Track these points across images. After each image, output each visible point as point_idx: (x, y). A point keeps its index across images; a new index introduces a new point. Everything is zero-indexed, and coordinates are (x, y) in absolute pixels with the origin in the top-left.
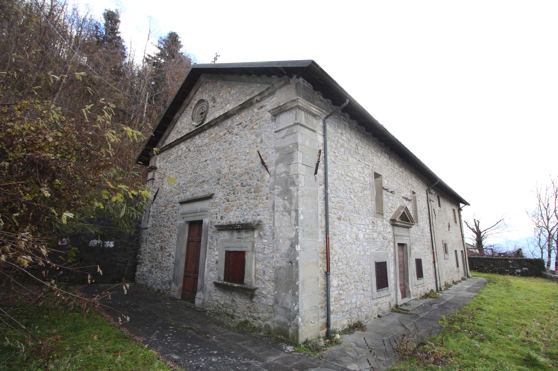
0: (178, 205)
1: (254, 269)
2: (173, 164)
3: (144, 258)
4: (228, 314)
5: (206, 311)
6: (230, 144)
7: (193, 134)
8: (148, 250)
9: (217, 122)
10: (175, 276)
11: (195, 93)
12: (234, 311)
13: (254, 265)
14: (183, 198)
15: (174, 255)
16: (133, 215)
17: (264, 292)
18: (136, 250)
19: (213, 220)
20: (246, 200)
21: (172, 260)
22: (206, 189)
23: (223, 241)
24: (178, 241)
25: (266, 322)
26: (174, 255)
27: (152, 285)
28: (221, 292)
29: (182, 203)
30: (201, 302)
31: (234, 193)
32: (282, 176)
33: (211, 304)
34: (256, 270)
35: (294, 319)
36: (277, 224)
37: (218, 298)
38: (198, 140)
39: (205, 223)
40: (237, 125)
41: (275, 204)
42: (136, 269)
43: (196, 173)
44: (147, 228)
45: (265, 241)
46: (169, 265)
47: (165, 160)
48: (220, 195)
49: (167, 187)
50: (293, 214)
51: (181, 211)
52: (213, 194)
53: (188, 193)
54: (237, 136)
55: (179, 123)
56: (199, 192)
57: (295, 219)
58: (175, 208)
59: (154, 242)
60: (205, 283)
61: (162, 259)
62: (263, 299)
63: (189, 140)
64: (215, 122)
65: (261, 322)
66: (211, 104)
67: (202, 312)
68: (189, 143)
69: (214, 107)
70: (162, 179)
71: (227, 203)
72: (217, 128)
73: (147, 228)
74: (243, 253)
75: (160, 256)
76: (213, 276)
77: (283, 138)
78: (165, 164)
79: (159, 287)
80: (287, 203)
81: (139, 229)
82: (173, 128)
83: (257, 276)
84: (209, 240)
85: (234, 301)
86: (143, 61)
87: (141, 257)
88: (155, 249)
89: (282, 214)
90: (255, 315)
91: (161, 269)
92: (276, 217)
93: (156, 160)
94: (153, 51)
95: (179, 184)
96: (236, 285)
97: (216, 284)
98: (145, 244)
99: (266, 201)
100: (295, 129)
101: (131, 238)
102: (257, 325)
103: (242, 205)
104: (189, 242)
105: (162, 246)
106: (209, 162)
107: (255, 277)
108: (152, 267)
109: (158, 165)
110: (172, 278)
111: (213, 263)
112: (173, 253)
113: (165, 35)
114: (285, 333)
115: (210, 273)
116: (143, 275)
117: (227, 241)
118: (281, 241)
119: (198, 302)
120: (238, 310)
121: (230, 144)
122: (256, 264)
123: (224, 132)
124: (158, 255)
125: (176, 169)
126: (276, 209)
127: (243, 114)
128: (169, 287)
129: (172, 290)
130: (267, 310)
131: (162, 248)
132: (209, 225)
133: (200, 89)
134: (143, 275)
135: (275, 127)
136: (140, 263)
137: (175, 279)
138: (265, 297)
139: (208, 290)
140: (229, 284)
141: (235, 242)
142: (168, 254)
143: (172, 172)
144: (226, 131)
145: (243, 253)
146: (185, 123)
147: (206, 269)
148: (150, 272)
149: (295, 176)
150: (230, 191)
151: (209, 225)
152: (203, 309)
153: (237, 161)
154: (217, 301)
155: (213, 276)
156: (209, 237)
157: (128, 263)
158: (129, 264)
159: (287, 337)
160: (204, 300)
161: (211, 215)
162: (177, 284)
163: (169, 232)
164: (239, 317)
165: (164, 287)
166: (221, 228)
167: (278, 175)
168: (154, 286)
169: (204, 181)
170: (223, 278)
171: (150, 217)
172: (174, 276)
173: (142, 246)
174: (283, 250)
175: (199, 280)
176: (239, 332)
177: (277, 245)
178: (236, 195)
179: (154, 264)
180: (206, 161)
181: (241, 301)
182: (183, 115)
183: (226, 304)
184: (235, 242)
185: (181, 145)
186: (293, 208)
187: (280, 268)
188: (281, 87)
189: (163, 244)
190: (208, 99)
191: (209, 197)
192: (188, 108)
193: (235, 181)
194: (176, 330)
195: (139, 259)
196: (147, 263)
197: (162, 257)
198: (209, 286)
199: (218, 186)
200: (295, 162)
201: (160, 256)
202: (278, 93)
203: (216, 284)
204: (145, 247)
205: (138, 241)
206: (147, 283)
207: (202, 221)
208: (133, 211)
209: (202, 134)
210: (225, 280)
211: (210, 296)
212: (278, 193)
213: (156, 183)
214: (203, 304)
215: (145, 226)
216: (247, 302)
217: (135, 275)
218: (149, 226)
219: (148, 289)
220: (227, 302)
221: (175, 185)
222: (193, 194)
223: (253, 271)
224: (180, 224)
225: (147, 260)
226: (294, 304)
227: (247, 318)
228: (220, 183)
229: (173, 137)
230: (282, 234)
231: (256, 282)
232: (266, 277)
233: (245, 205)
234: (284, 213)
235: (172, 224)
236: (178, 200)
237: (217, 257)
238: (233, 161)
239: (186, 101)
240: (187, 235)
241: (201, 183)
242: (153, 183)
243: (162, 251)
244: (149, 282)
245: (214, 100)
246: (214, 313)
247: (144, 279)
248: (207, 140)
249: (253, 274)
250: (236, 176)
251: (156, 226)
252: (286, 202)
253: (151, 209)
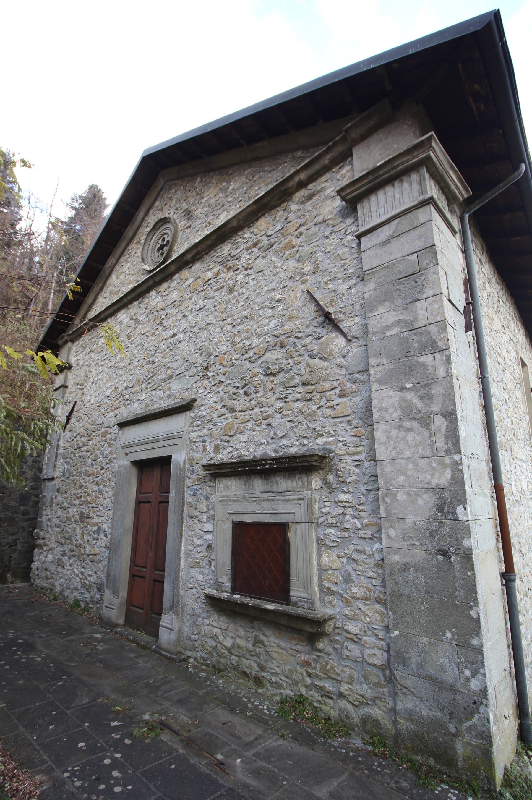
0: (116, 429)
1: (315, 567)
2: (103, 353)
3: (48, 536)
4: (245, 673)
5: (186, 660)
6: (231, 291)
7: (144, 287)
8: (56, 521)
9: (198, 253)
10: (112, 573)
11: (147, 214)
12: (262, 668)
13: (315, 556)
14: (125, 414)
15: (108, 531)
16: (23, 448)
17: (351, 627)
18: (33, 521)
19: (196, 456)
20: (280, 404)
21: (103, 541)
22: (177, 391)
23: (224, 500)
24: (116, 502)
25: (365, 710)
26: (108, 531)
27: (63, 590)
28: (223, 618)
29: (122, 425)
30: (173, 636)
31: (246, 393)
32: (389, 333)
33: (197, 644)
34: (322, 570)
35: (472, 715)
36: (381, 453)
37: (215, 630)
38: (154, 299)
39: (178, 463)
40: (248, 249)
41: (374, 403)
42: (32, 556)
43: (153, 362)
44: (53, 479)
45: (343, 497)
46: (97, 551)
47: (87, 350)
48: (209, 402)
49: (91, 397)
50: (439, 423)
51: (122, 441)
52: (195, 400)
53: (136, 405)
54: (249, 272)
55: (114, 276)
56: (161, 398)
57: (447, 438)
58: (109, 436)
59: (66, 505)
60: (182, 593)
61: (83, 539)
62: (351, 646)
63: (136, 303)
64: (194, 252)
65: (350, 707)
66: (181, 224)
67: (175, 661)
68: (135, 308)
69: (190, 227)
70: (82, 385)
71: (228, 415)
72: (197, 266)
73: (53, 479)
74: (281, 529)
75: (79, 532)
76: (200, 578)
77: (387, 242)
78: (87, 357)
79: (76, 594)
80: (413, 398)
81: (39, 481)
82: (102, 289)
83: (326, 584)
84: (189, 499)
85: (261, 642)
86: (48, 228)
87: (42, 534)
88: (68, 519)
89: (400, 428)
90: (328, 685)
91: (80, 557)
92: (377, 435)
93: (70, 349)
94: (65, 214)
95: (116, 389)
96: (271, 607)
97: (215, 603)
98: (48, 509)
99: (339, 400)
100: (421, 215)
101: (24, 498)
102: (333, 713)
103: (269, 416)
104: (139, 503)
105: (82, 513)
106: (181, 336)
107: (321, 587)
108: (64, 554)
109: (73, 361)
110: (104, 579)
111: (199, 549)
112: (105, 526)
113: (82, 190)
114: (444, 755)
115: (193, 570)
116: (46, 569)
117: (235, 500)
118: (401, 496)
119: (166, 637)
120: (273, 666)
121: (231, 291)
122: (319, 555)
123: (215, 270)
124: (74, 529)
125: (110, 361)
126: (376, 415)
127: (263, 223)
128: (98, 596)
129: (105, 604)
130: (364, 677)
131: (83, 518)
132: (187, 466)
133: (157, 203)
134: (46, 569)
135: (354, 228)
136: (40, 546)
137: (111, 581)
138: (356, 640)
139: (188, 609)
140: (249, 601)
141: (255, 503)
142: (95, 528)
143: (100, 369)
144: (218, 268)
145: (281, 529)
146: (128, 272)
147: (183, 562)
148: (60, 564)
149: (433, 329)
150: (235, 390)
151: (187, 466)
152: (180, 653)
153: (252, 323)
154: (215, 637)
155: (200, 578)
156: (187, 492)
157: (18, 545)
158: (19, 547)
159: (451, 762)
160: (180, 631)
161: (188, 446)
162: (115, 592)
163: (97, 484)
164: (278, 686)
165: (87, 595)
166: (218, 471)
167: (375, 334)
168: (67, 593)
169: (171, 377)
170: (228, 585)
171: (60, 457)
172: (108, 575)
173: (44, 513)
174: (409, 520)
175: (167, 587)
176: (294, 738)
177: (387, 506)
178: (253, 396)
179: (67, 548)
180: (174, 335)
181: (282, 644)
182: (122, 259)
183: (239, 647)
184: (255, 503)
185: (119, 315)
186: (436, 408)
187: (405, 567)
188: (364, 137)
189: (85, 509)
190: (175, 217)
191: (186, 407)
192: (133, 245)
193: (248, 365)
194: (130, 736)
195: (39, 538)
196: (54, 545)
197: (83, 534)
198: (192, 600)
199: (206, 382)
200: (429, 292)
201: (79, 532)
202: (357, 153)
203: (215, 603)
204: (50, 516)
205: (37, 503)
206: (53, 585)
207: (170, 457)
208: (23, 439)
209: (165, 285)
210: (234, 590)
211: (195, 623)
212: (379, 375)
213: (71, 393)
214: (178, 640)
215: (50, 476)
216: (299, 648)
217: (31, 569)
218: (57, 474)
219: (55, 599)
220: (242, 642)
221: (108, 392)
222: (147, 406)
223: (315, 572)
224: (120, 467)
225: (53, 540)
226: (468, 673)
227: (303, 691)
228: (210, 374)
229: (103, 303)
230: (402, 478)
231: (322, 600)
232: (354, 590)
233: (279, 416)
234: (407, 424)
235: (102, 468)
236: (114, 421)
237: (209, 537)
238: (240, 324)
239: (129, 233)
240: (135, 489)
241: (163, 381)
242: (64, 393)
243: (82, 522)
244: (57, 583)
245: (188, 214)
246: (207, 665)
247: (47, 578)
248: (175, 295)
249: (316, 579)
250: (251, 354)
251: (71, 474)
252: (411, 397)
253: (61, 443)
